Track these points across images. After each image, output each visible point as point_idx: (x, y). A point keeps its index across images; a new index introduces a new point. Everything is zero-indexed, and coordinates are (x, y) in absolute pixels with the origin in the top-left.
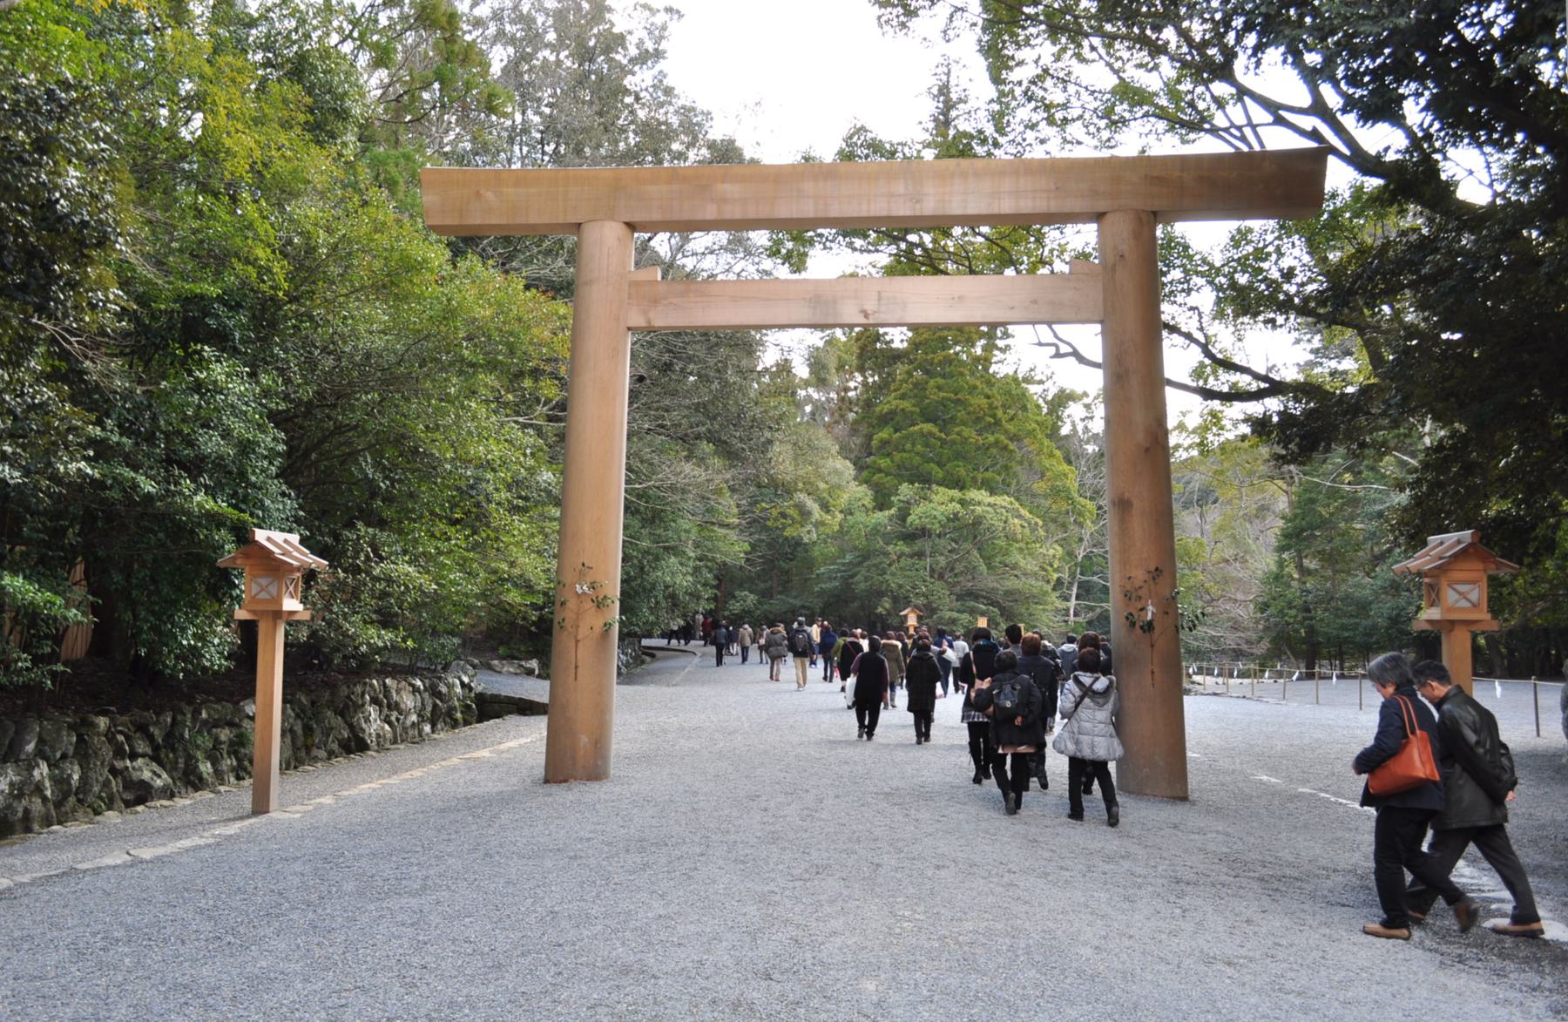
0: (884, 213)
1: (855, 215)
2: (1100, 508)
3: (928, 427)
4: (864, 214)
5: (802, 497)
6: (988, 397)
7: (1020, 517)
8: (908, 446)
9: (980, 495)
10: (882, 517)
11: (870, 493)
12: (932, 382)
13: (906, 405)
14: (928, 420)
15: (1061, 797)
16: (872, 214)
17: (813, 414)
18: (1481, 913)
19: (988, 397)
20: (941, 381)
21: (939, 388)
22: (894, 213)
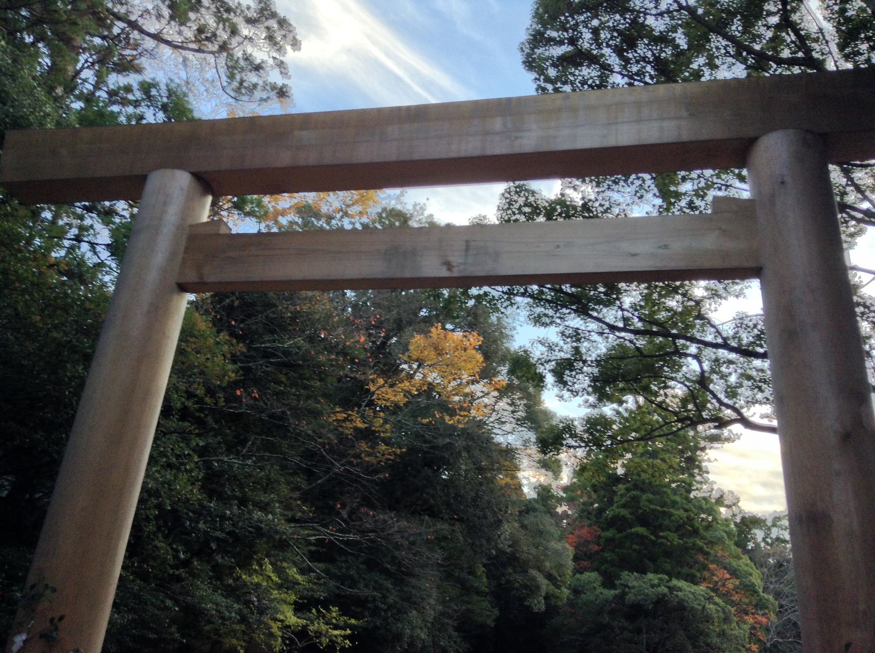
0: (476, 153)
1: (443, 156)
2: (781, 606)
3: (640, 530)
4: (454, 155)
5: (533, 572)
6: (686, 510)
7: (716, 604)
8: (627, 544)
9: (681, 584)
10: (610, 593)
11: (600, 578)
12: (644, 497)
13: (624, 512)
14: (642, 526)
15: (774, 474)
16: (462, 154)
17: (24, 289)
18: (429, 220)
19: (686, 510)
20: (651, 496)
21: (650, 501)
22: (489, 152)
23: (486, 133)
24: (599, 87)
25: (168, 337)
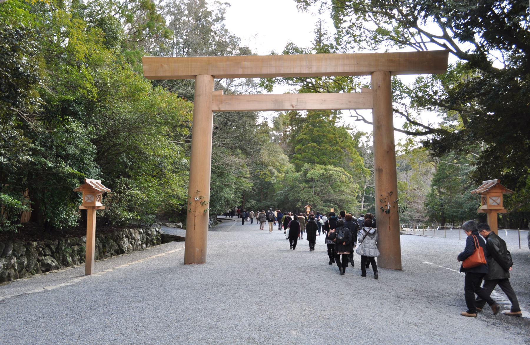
0: (299, 72)
1: (289, 72)
2: (372, 171)
3: (314, 144)
4: (292, 72)
5: (271, 168)
6: (334, 134)
7: (345, 174)
8: (307, 151)
9: (331, 167)
11: (294, 166)
12: (315, 129)
13: (306, 137)
14: (314, 142)
16: (295, 72)
19: (334, 134)
20: (318, 129)
21: (318, 131)
22: (302, 72)
23: (301, 66)
24: (324, 3)
25: (507, 329)
